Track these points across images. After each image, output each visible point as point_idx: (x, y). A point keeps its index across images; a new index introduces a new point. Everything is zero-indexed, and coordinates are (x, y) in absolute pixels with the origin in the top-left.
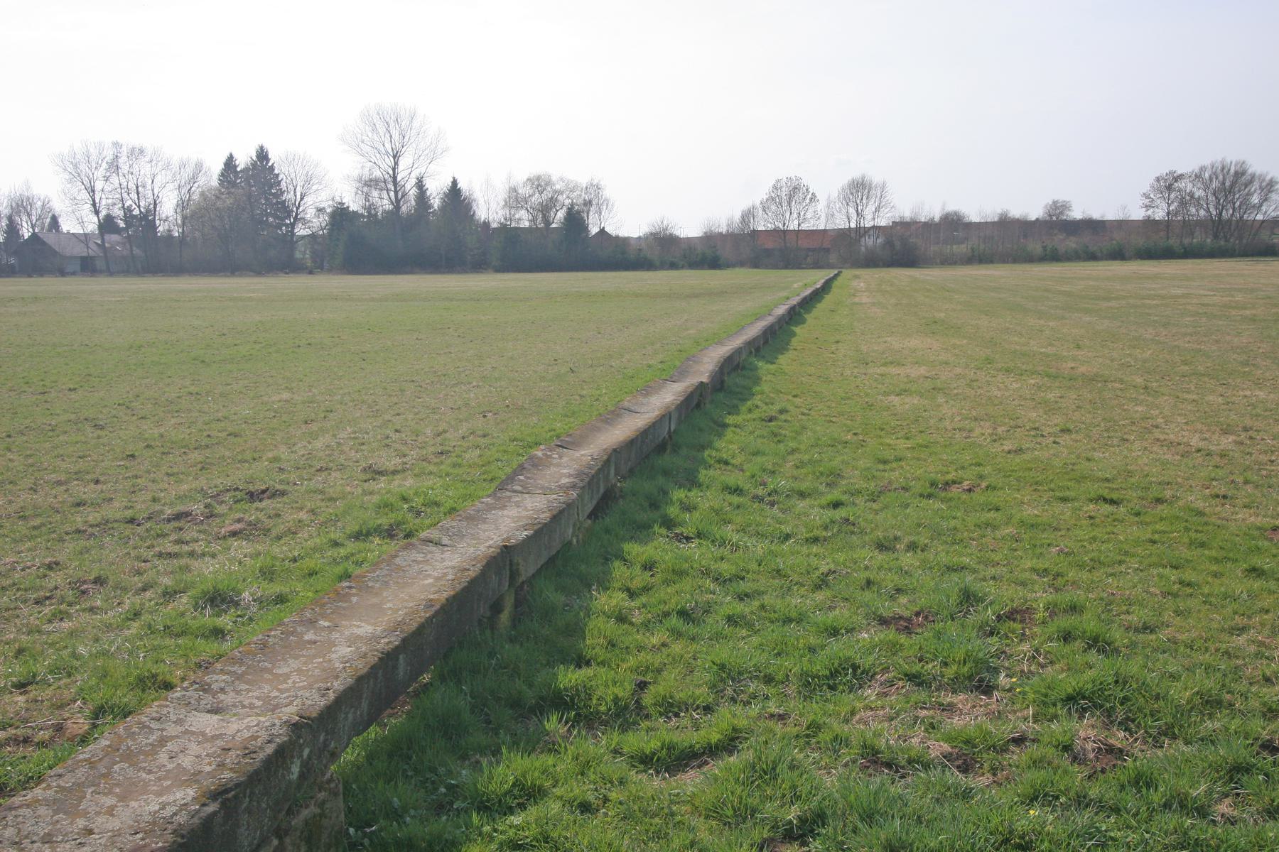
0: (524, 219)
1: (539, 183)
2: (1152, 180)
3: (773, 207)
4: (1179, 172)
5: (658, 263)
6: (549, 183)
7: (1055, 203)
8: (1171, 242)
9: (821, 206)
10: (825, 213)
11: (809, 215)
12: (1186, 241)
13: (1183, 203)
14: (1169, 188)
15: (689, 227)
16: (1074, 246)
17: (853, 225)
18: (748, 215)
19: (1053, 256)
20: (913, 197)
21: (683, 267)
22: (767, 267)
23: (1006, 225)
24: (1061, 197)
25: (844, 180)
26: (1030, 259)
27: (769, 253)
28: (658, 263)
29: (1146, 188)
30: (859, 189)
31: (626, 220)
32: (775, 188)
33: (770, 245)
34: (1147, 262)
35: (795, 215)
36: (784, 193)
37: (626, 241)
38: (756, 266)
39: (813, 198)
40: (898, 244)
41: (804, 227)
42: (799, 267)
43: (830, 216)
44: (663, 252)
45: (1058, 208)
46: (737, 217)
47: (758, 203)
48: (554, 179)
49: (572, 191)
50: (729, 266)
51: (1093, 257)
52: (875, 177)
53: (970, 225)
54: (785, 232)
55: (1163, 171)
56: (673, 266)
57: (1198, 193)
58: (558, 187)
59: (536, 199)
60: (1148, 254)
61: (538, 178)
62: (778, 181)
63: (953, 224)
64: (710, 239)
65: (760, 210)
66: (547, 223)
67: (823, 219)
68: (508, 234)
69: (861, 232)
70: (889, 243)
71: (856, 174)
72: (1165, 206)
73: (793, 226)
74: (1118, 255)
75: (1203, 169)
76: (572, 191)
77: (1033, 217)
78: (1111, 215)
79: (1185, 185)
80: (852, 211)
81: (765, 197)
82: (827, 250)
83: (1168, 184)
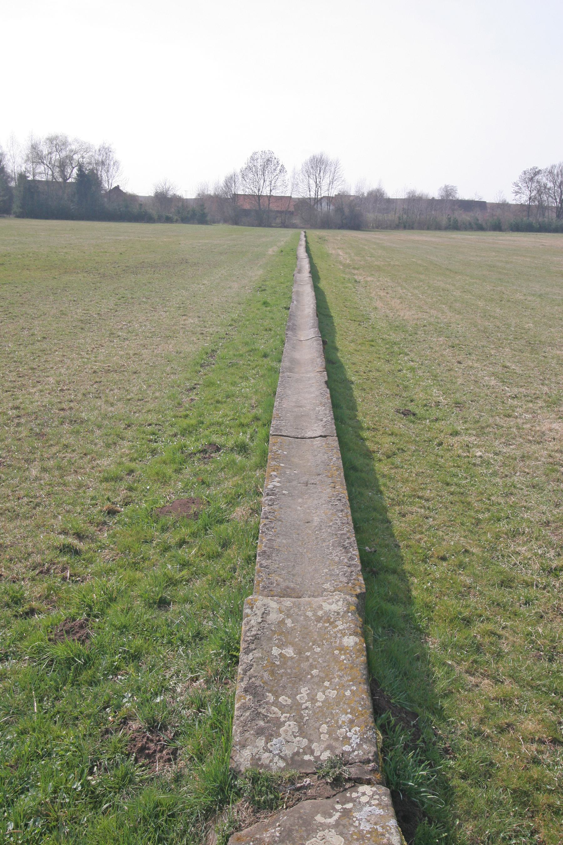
0: (43, 174)
1: (57, 143)
2: (520, 173)
3: (251, 175)
4: (539, 168)
5: (156, 217)
6: (65, 144)
7: (446, 187)
8: (531, 219)
9: (288, 176)
10: (292, 184)
11: (279, 183)
12: (541, 219)
13: (539, 192)
14: (531, 179)
15: (187, 190)
16: (468, 219)
17: (313, 195)
18: (230, 181)
19: (455, 226)
20: (353, 179)
21: (177, 221)
22: (244, 225)
23: (414, 201)
24: (450, 183)
25: (307, 157)
26: (438, 228)
27: (246, 213)
28: (156, 217)
29: (516, 179)
30: (318, 165)
31: (135, 179)
32: (252, 159)
33: (247, 207)
34: (516, 234)
35: (267, 183)
36: (259, 163)
37: (133, 198)
38: (236, 223)
39: (282, 170)
40: (347, 211)
41: (274, 193)
42: (270, 226)
43: (295, 185)
44: (166, 209)
45: (448, 192)
46: (222, 183)
47: (238, 171)
48: (70, 140)
49: (86, 151)
50: (213, 222)
51: (480, 228)
52: (331, 155)
53: (389, 201)
54: (259, 197)
55: (528, 166)
56: (168, 220)
57: (550, 185)
58: (73, 147)
59: (55, 157)
60: (517, 228)
61: (56, 138)
62: (255, 153)
63: (377, 198)
64: (203, 201)
65: (240, 177)
66: (65, 179)
67: (290, 187)
68: (29, 187)
69: (317, 201)
70: (339, 210)
71: (316, 151)
72: (528, 193)
73: (266, 192)
74: (497, 227)
75: (553, 167)
76: (86, 151)
77: (430, 196)
78: (490, 198)
79: (543, 179)
80: (312, 182)
81: (244, 166)
82: (292, 213)
83: (532, 176)
